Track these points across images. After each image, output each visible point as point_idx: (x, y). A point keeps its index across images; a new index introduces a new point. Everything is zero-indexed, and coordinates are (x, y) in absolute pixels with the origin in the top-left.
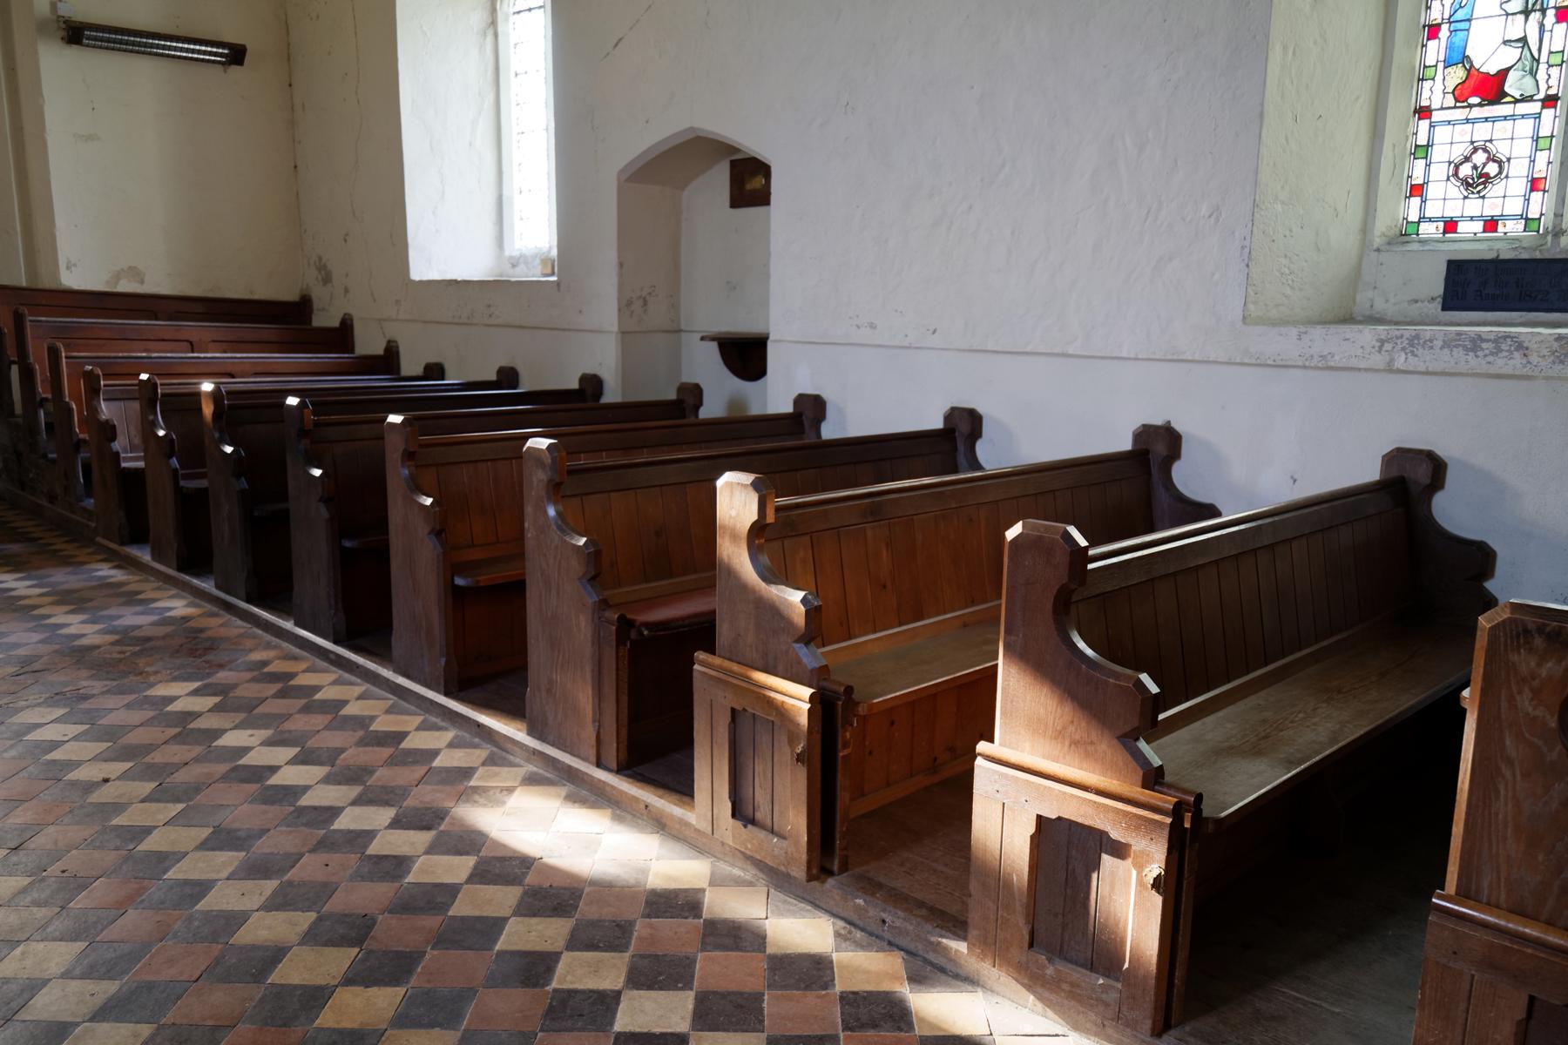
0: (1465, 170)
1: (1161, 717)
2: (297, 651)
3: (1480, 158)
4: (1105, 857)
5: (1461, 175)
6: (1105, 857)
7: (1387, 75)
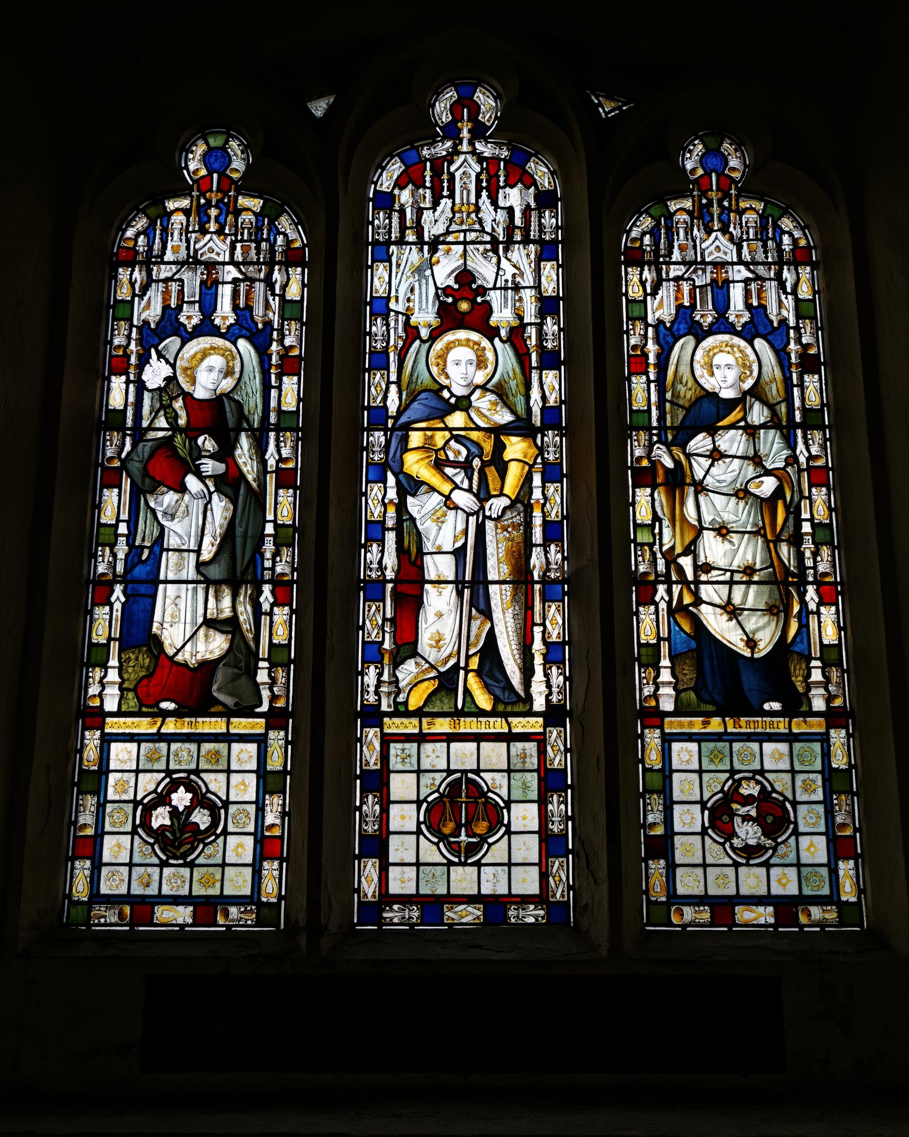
2: (603, 873)
3: (181, 798)
5: (155, 825)
7: (830, 308)
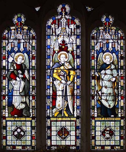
0: (16, 133)
1: (64, 9)
3: (19, 130)
4: (17, 134)
5: (15, 134)
6: (17, 134)
